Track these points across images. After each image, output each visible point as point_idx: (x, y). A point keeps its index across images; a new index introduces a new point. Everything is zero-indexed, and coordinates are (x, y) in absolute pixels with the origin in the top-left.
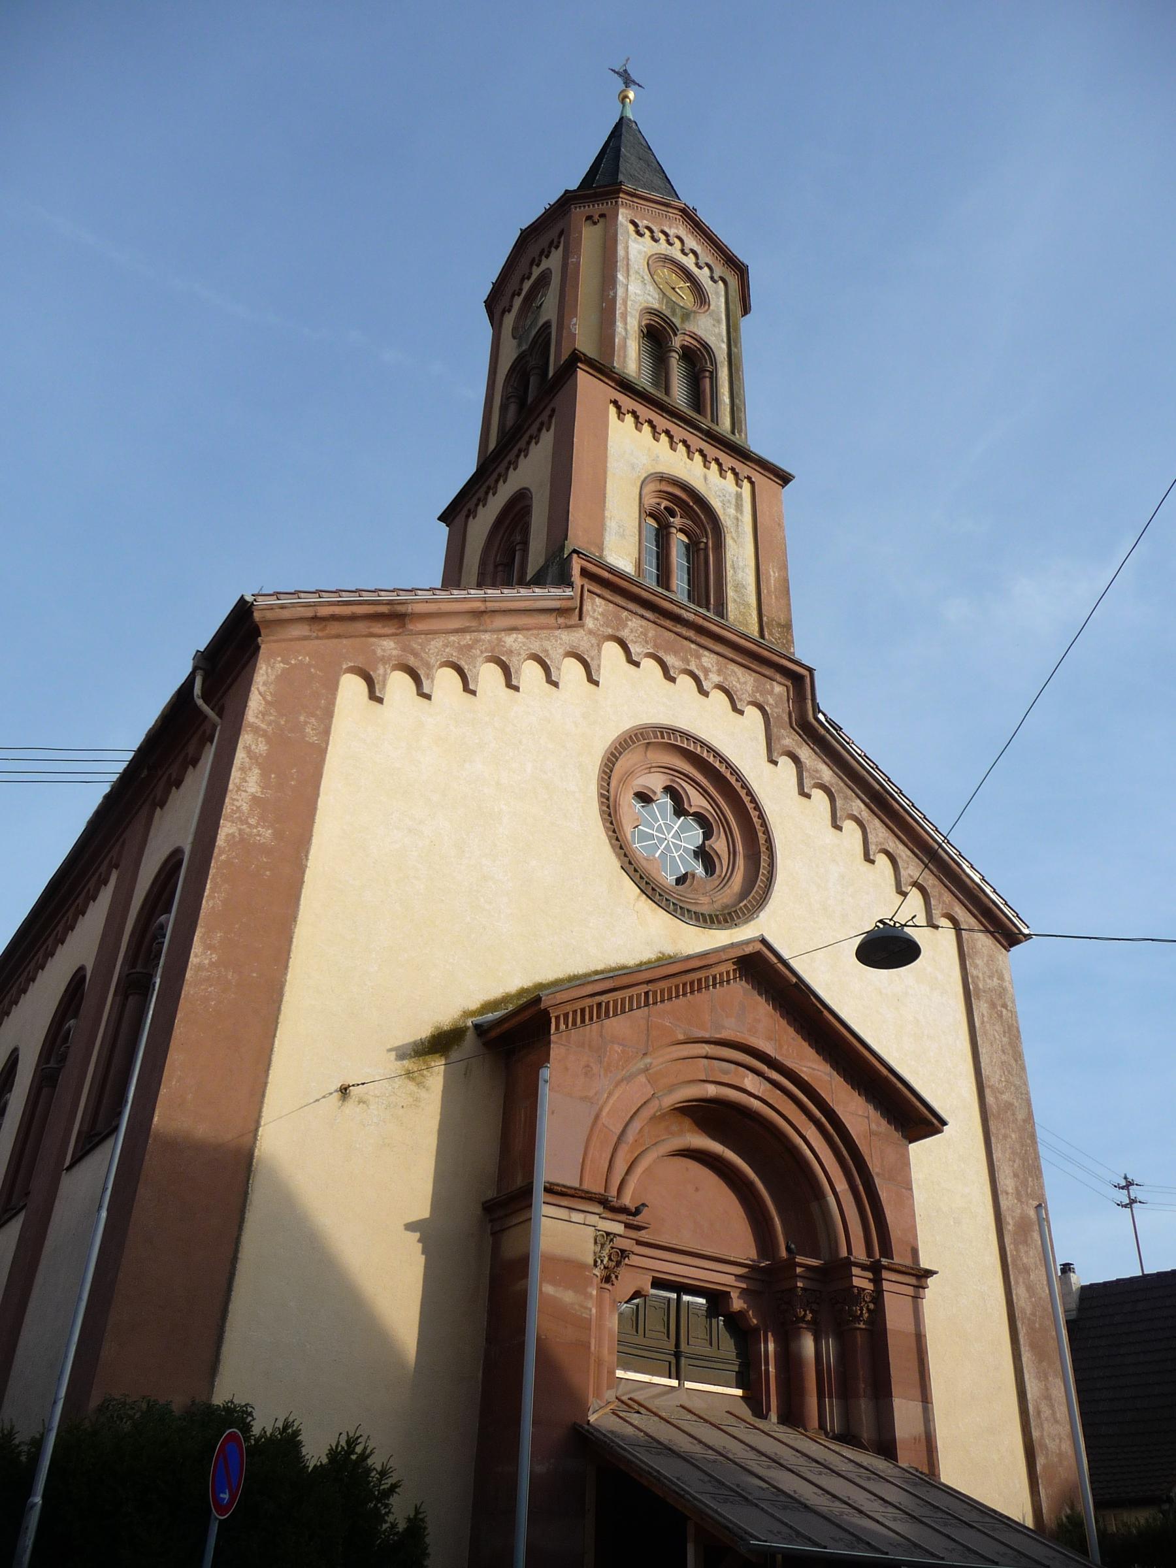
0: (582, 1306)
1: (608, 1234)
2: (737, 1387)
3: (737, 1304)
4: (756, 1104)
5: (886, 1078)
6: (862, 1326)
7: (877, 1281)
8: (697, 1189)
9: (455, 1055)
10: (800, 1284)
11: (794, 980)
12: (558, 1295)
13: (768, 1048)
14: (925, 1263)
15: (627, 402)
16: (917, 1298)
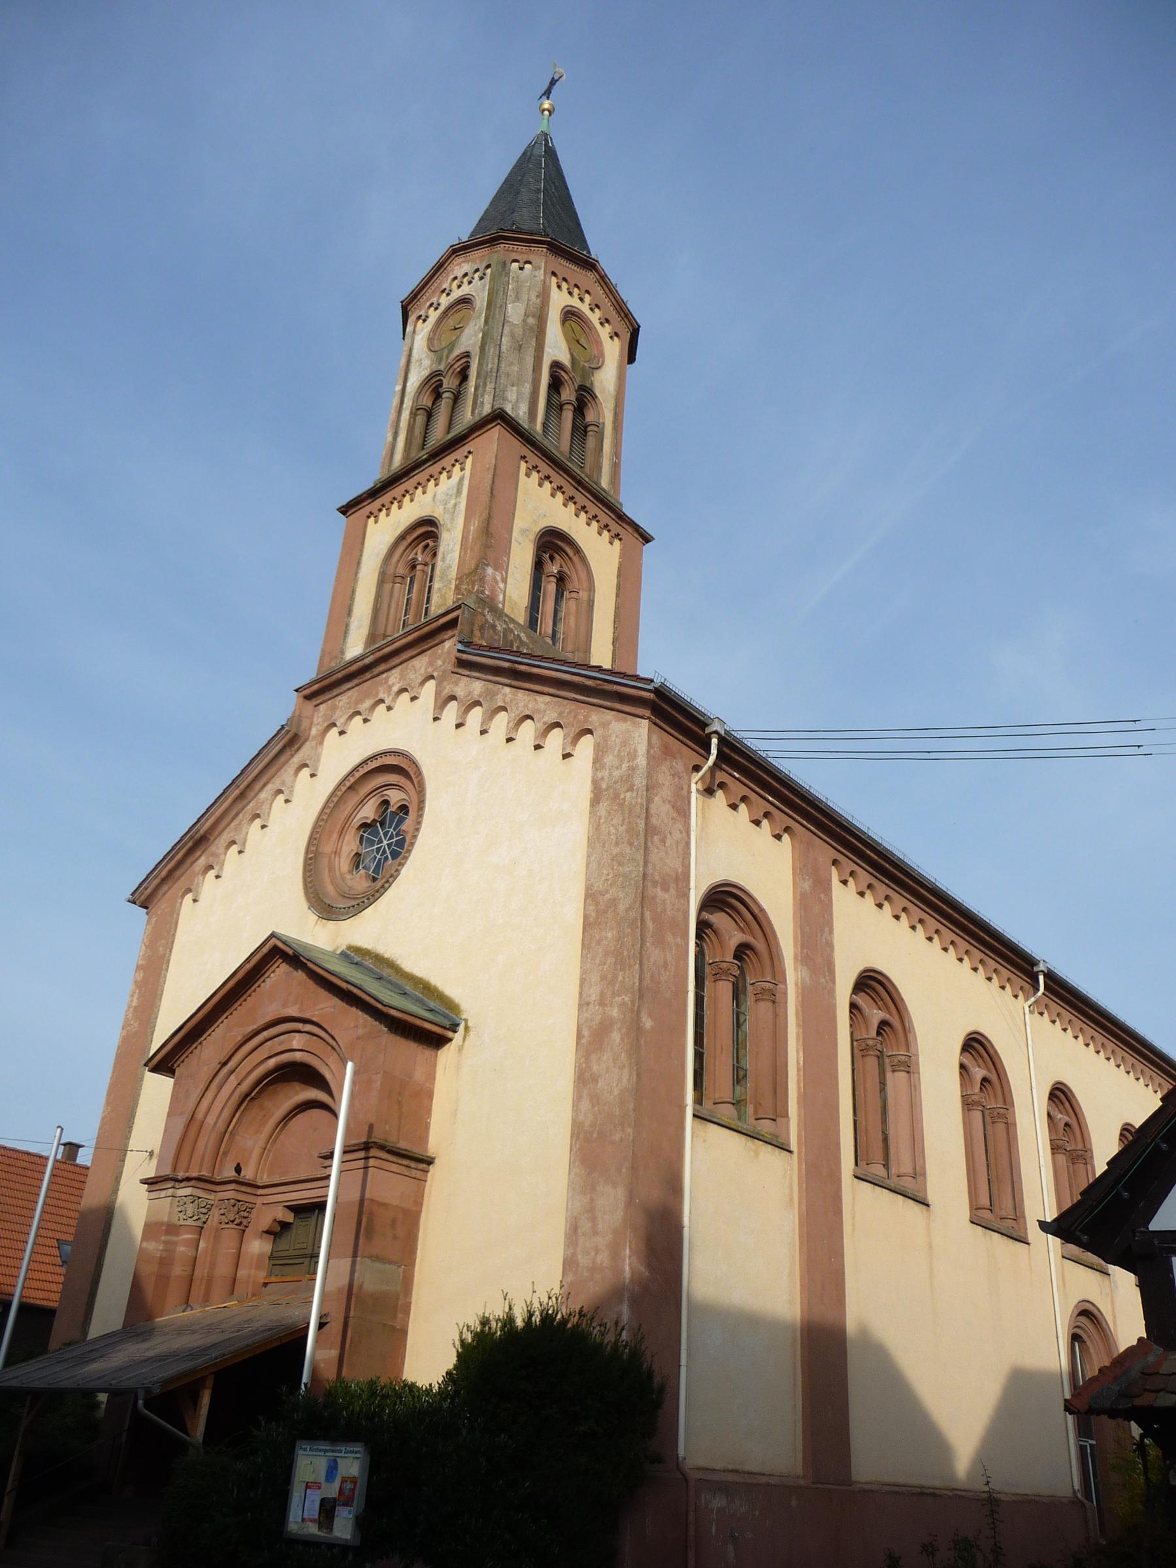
15: (534, 459)
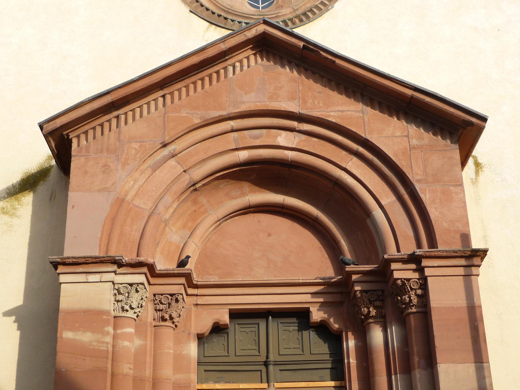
0: (99, 342)
1: (131, 285)
2: (332, 380)
3: (317, 315)
4: (290, 155)
5: (412, 97)
6: (414, 310)
7: (420, 270)
8: (269, 235)
9: (42, 188)
10: (357, 288)
11: (301, 44)
12: (77, 337)
13: (293, 107)
14: (476, 244)
16: (468, 276)
